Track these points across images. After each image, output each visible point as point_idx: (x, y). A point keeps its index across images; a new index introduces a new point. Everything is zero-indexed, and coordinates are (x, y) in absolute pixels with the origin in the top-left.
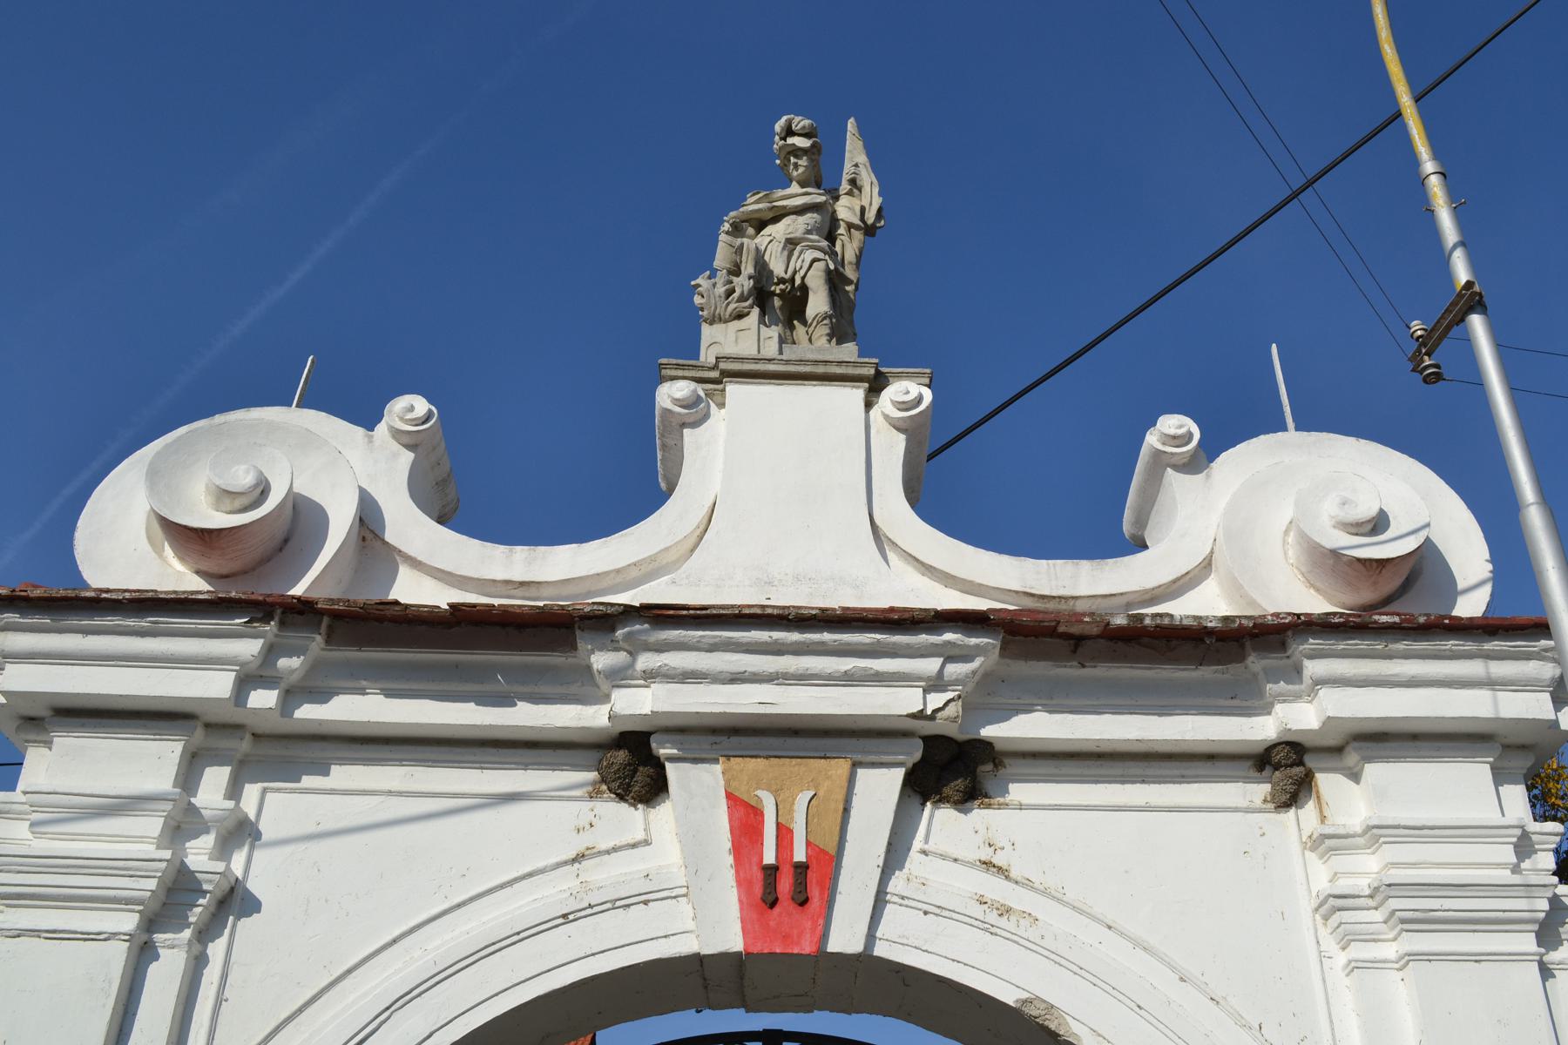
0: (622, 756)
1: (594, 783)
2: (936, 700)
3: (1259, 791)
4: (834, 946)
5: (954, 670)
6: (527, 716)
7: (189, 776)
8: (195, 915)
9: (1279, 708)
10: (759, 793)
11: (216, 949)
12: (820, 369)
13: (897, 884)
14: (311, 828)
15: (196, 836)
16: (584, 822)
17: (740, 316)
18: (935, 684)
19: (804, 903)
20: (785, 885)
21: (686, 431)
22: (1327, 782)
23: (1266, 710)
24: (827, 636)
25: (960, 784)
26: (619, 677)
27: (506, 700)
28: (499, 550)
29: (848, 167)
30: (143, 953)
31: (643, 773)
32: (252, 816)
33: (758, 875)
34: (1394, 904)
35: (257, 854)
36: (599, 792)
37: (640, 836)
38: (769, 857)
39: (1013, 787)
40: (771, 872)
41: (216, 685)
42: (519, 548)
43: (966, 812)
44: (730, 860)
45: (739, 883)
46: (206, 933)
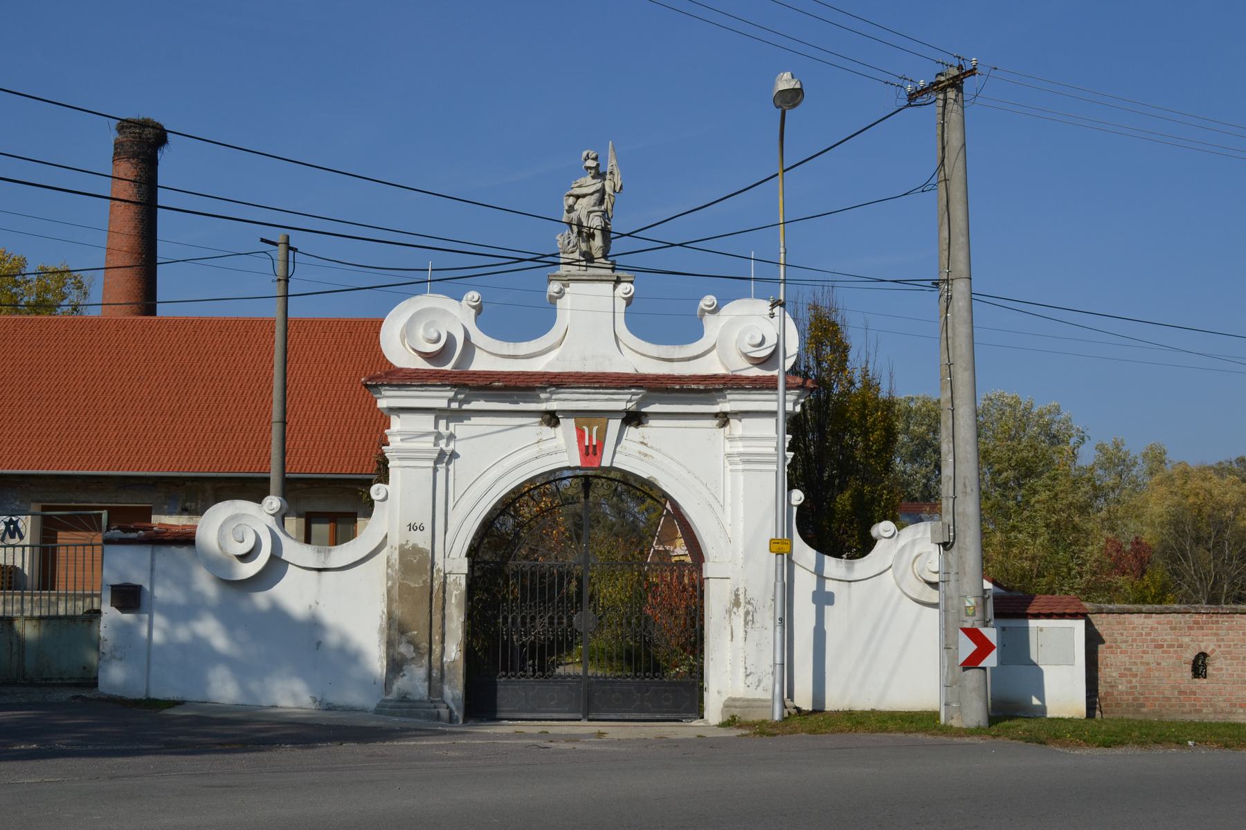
1: (541, 422)
2: (629, 405)
3: (716, 422)
4: (603, 465)
5: (634, 397)
6: (522, 406)
8: (446, 460)
9: (720, 404)
11: (451, 467)
12: (599, 278)
13: (619, 448)
17: (573, 252)
20: (591, 450)
21: (558, 300)
23: (718, 404)
24: (601, 391)
25: (636, 422)
26: (548, 400)
27: (517, 403)
28: (505, 344)
29: (609, 165)
30: (435, 470)
31: (553, 421)
32: (453, 432)
36: (542, 424)
37: (554, 436)
38: (587, 444)
40: (587, 447)
41: (443, 404)
42: (511, 343)
43: (637, 428)
44: (577, 443)
45: (579, 449)
46: (448, 463)
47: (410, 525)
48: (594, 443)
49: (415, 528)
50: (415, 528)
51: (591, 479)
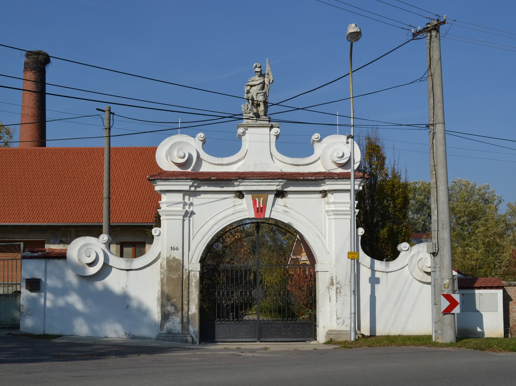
0: (238, 193)
1: (235, 196)
2: (278, 187)
4: (266, 217)
5: (280, 184)
7: (184, 199)
8: (189, 215)
10: (256, 198)
12: (263, 126)
13: (273, 209)
14: (200, 203)
15: (186, 205)
16: (234, 201)
18: (278, 185)
19: (262, 212)
20: (260, 210)
22: (329, 195)
24: (264, 181)
26: (238, 186)
27: (223, 187)
28: (217, 158)
29: (267, 70)
30: (184, 220)
33: (256, 209)
34: (333, 212)
35: (194, 207)
37: (241, 203)
38: (258, 207)
39: (288, 195)
40: (258, 208)
42: (220, 158)
44: (253, 206)
46: (190, 217)
47: (172, 247)
48: (261, 206)
49: (174, 249)
50: (174, 249)
51: (260, 224)
